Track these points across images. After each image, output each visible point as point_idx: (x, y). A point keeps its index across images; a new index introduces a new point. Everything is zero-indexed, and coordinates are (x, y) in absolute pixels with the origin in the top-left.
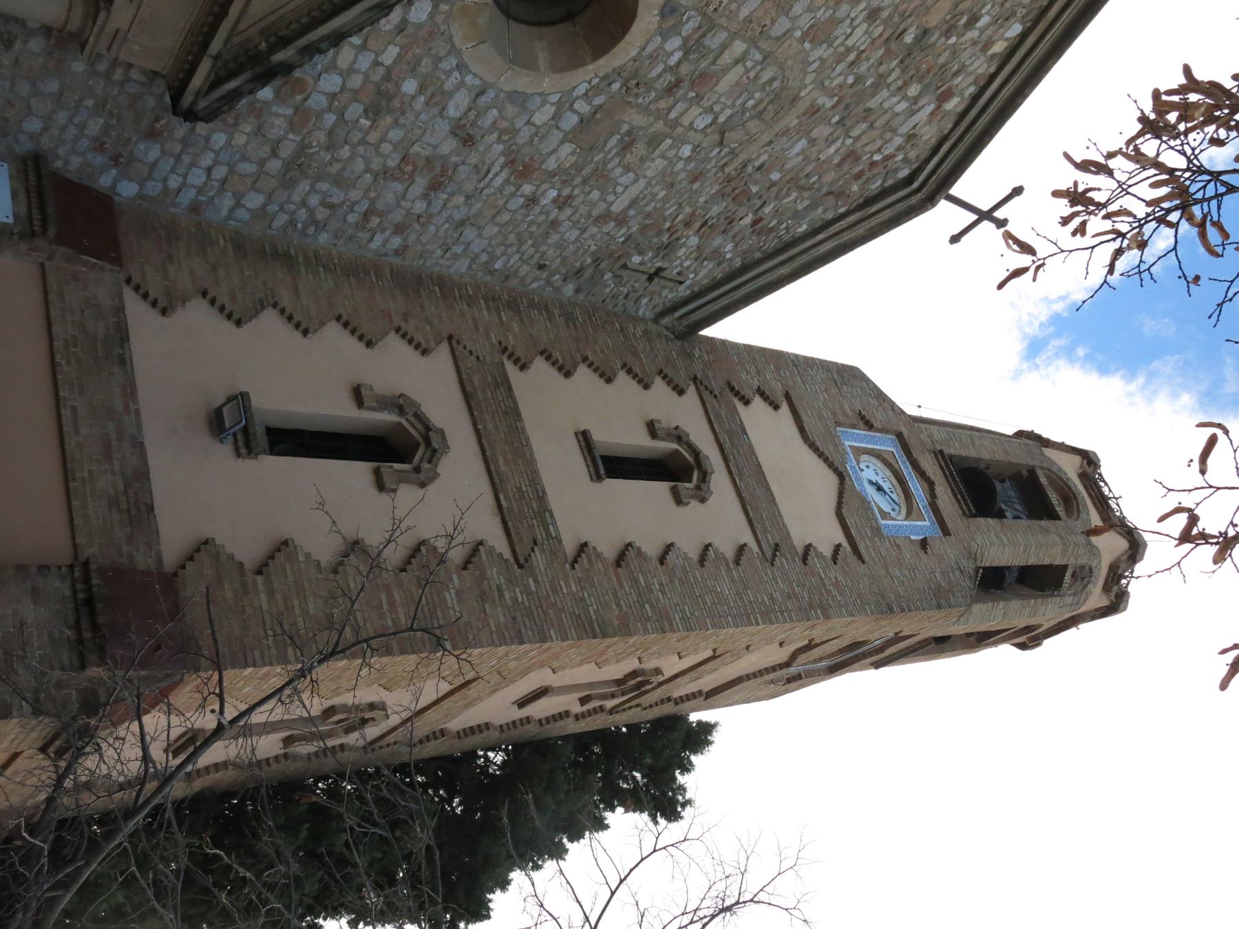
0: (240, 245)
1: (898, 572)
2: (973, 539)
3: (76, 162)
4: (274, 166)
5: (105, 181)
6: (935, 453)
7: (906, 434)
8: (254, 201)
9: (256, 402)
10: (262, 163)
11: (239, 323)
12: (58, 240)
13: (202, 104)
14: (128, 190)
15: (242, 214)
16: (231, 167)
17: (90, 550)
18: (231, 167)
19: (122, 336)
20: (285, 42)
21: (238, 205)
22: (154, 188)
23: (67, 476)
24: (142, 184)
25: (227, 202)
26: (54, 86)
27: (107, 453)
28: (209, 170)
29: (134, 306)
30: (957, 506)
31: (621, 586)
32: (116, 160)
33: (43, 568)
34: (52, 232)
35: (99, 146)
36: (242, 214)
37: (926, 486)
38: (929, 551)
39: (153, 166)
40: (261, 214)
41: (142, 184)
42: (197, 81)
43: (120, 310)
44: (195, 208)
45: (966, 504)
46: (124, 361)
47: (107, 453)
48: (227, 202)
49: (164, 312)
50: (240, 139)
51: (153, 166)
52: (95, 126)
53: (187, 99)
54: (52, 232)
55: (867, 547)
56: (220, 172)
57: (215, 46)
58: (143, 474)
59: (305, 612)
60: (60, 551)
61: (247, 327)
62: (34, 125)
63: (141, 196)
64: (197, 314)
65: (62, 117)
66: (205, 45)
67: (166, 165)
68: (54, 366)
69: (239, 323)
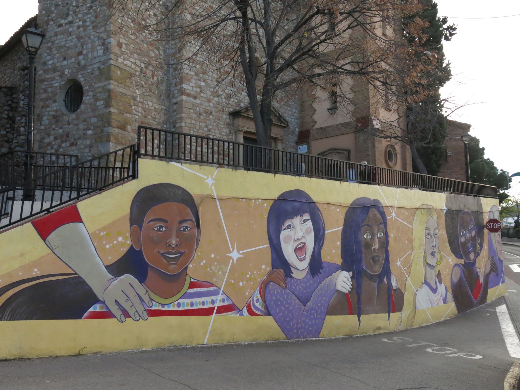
0: (302, 111)
3: (295, 138)
4: (289, 109)
5: (297, 133)
8: (294, 110)
9: (329, 107)
10: (289, 111)
11: (316, 110)
12: (308, 139)
13: (286, 123)
14: (297, 130)
15: (297, 112)
16: (291, 115)
17: (353, 131)
18: (291, 115)
19: (321, 128)
20: (276, 115)
21: (295, 112)
22: (296, 126)
23: (343, 134)
24: (296, 128)
25: (295, 114)
26: (287, 142)
27: (339, 129)
28: (292, 119)
29: (316, 126)
31: (357, 30)
32: (294, 132)
33: (355, 137)
34: (307, 140)
35: (293, 135)
36: (297, 112)
39: (293, 127)
40: (296, 109)
41: (296, 128)
42: (283, 125)
43: (317, 129)
44: (297, 119)
46: (325, 128)
47: (339, 129)
48: (295, 114)
49: (316, 122)
50: (287, 115)
51: (293, 127)
52: (290, 136)
53: (286, 126)
54: (307, 140)
56: (292, 117)
57: (279, 124)
58: (342, 124)
59: (362, 98)
60: (353, 134)
61: (316, 109)
62: (292, 144)
63: (298, 128)
64: (315, 117)
65: (290, 141)
66: (278, 125)
67: (293, 125)
68: (327, 137)
69: (316, 110)
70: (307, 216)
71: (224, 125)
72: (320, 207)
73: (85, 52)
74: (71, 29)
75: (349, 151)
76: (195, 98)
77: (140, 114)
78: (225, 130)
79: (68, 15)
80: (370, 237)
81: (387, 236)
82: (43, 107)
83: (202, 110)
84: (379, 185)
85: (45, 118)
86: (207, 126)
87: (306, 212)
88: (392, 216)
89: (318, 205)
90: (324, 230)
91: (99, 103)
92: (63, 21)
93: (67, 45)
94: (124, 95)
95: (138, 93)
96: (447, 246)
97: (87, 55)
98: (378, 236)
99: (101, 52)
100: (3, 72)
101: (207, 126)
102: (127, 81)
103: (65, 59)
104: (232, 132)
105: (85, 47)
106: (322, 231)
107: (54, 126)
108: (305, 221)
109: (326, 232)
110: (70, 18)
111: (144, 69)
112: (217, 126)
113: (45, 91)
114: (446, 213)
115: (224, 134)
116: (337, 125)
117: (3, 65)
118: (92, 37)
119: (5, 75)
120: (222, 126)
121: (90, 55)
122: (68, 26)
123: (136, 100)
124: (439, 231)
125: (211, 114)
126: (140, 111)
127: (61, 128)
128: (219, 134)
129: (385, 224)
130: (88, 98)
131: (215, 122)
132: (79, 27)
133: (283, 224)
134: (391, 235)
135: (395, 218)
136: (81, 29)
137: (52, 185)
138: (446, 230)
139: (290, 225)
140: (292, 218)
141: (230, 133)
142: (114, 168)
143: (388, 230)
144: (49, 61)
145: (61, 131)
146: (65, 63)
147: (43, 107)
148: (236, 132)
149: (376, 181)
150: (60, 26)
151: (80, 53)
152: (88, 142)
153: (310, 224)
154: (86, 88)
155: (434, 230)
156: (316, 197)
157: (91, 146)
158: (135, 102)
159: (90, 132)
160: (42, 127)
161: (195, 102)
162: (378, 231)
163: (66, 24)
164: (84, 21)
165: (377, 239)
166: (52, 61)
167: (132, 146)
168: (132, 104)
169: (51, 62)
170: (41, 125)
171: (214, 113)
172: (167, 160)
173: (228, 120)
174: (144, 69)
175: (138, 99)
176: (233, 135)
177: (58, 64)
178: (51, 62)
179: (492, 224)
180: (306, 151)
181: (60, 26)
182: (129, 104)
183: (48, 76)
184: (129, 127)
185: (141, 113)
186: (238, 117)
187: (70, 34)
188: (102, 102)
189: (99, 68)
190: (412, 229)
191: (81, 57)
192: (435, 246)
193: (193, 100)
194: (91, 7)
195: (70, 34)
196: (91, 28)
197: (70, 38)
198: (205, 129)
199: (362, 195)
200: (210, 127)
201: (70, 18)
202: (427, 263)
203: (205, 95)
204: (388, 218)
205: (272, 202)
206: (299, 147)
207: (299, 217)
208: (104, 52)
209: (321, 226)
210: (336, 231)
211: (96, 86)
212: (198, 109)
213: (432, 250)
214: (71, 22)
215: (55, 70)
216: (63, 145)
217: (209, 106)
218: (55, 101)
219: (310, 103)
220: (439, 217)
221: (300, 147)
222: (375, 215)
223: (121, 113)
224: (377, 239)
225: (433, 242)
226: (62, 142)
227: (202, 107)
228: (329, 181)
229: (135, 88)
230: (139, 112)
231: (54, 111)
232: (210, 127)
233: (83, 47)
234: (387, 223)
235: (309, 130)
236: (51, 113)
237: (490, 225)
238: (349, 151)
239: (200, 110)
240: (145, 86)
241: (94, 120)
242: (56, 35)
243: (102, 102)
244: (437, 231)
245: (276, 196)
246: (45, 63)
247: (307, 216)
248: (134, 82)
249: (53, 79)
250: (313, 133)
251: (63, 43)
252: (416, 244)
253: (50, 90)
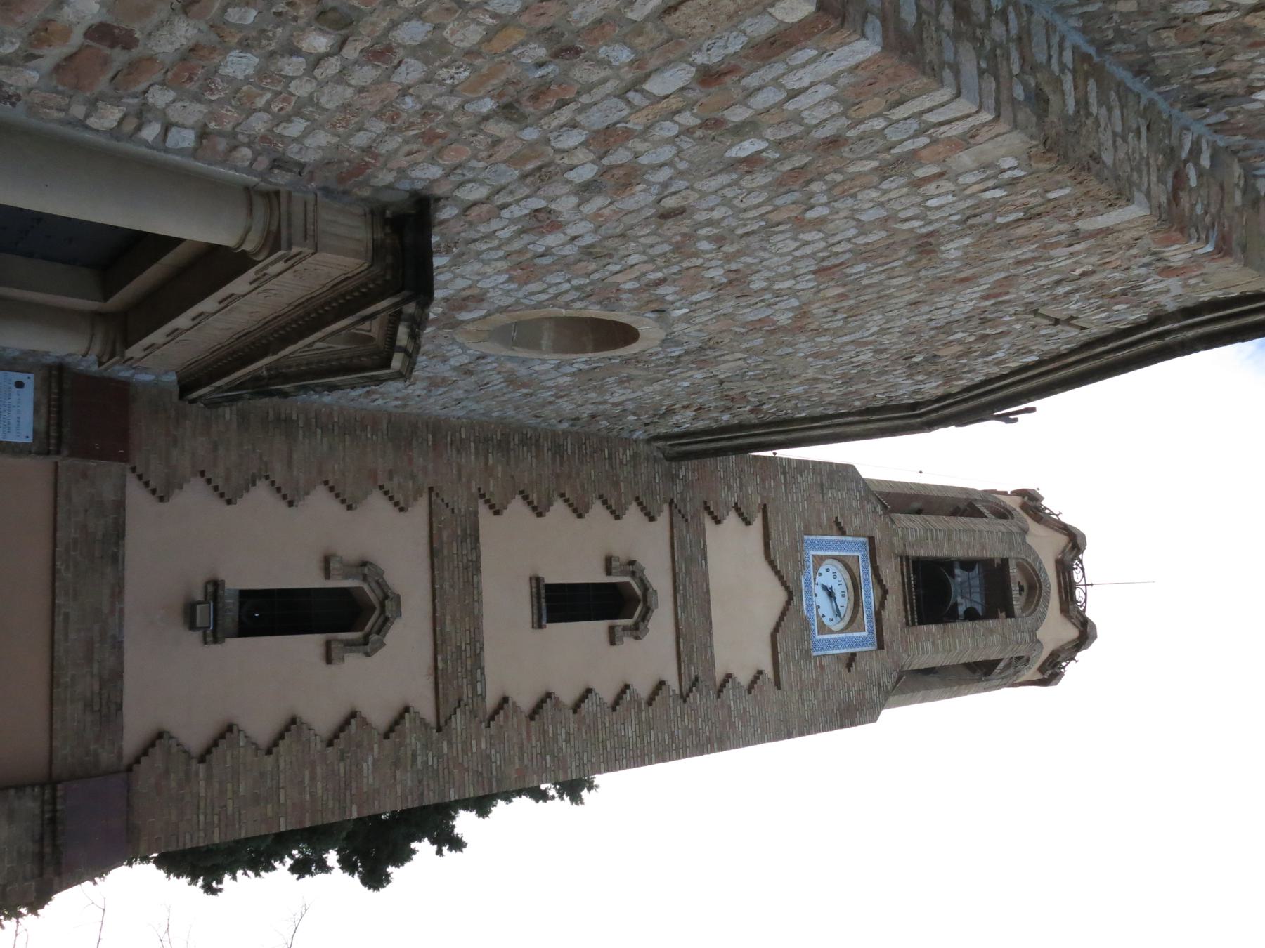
1: (811, 694)
2: (906, 650)
6: (901, 558)
7: (877, 541)
19: (118, 533)
23: (53, 682)
29: (136, 495)
30: (903, 614)
34: (65, 452)
37: (880, 592)
38: (853, 669)
43: (120, 506)
45: (912, 614)
46: (116, 560)
55: (789, 672)
58: (118, 674)
59: (235, 792)
64: (193, 496)
68: (54, 572)
71: (367, 150)
76: (709, 77)
78: (322, 139)
83: (582, 72)
104: (281, 179)
112: (388, 112)
115: (296, 128)
116: (118, 646)
120: (361, 139)
125: (509, 111)
128: (311, 100)
131: (427, 112)
141: (279, 163)
148: (272, 197)
161: (684, 58)
171: (499, 128)
172: (1079, 541)
173: (386, 178)
176: (250, 170)
186: (377, 250)
193: (711, 57)
198: (413, 33)
200: (412, 71)
206: (29, 380)
212: (623, 55)
217: (574, 125)
219: (279, 475)
221: (28, 394)
227: (610, 86)
235: (124, 458)
239: (605, 63)
250: (105, 474)
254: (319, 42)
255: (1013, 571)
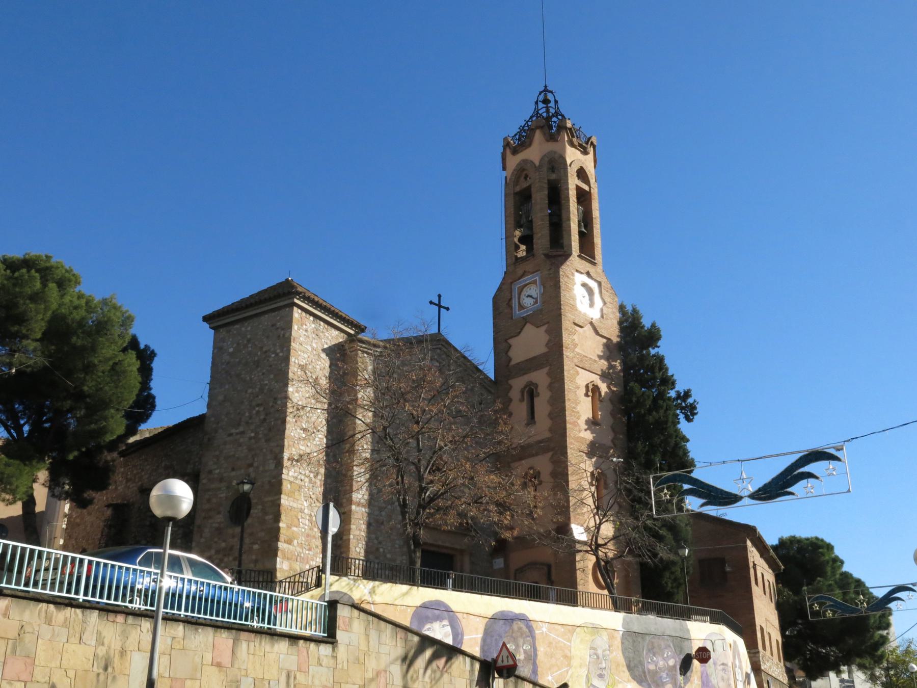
70: (446, 622)
72: (460, 616)
73: (255, 464)
74: (241, 440)
75: (549, 567)
77: (306, 527)
79: (239, 425)
80: (514, 648)
81: (535, 649)
82: (205, 518)
84: (583, 607)
85: (207, 530)
86: (377, 538)
87: (446, 619)
88: (541, 631)
89: (457, 614)
90: (463, 635)
91: (267, 518)
92: (233, 431)
93: (237, 456)
94: (292, 508)
95: (306, 505)
96: (624, 672)
97: (258, 467)
98: (524, 648)
99: (272, 466)
100: (139, 467)
101: (377, 538)
102: (296, 493)
103: (233, 469)
105: (256, 459)
106: (460, 636)
107: (216, 540)
108: (444, 626)
109: (465, 637)
110: (241, 429)
111: (313, 479)
113: (209, 500)
114: (623, 635)
117: (141, 458)
118: (264, 450)
119: (143, 470)
121: (261, 468)
122: (239, 436)
123: (304, 513)
124: (611, 653)
126: (307, 524)
127: (224, 541)
129: (533, 637)
130: (256, 511)
132: (250, 438)
133: (424, 627)
134: (541, 649)
135: (546, 634)
136: (253, 441)
137: (297, 583)
138: (623, 653)
139: (430, 628)
140: (432, 623)
142: (381, 569)
143: (537, 644)
144: (215, 469)
145: (223, 545)
146: (233, 474)
147: (205, 518)
149: (577, 603)
150: (231, 435)
151: (250, 465)
152: (254, 557)
153: (448, 629)
154: (254, 501)
155: (604, 651)
156: (454, 608)
157: (256, 561)
158: (302, 514)
159: (256, 547)
160: (203, 540)
162: (524, 644)
163: (237, 434)
164: (257, 433)
165: (522, 650)
166: (218, 470)
167: (318, 567)
168: (300, 517)
169: (217, 471)
170: (201, 537)
174: (313, 479)
175: (306, 511)
177: (225, 475)
178: (217, 471)
179: (701, 653)
180: (502, 566)
181: (231, 435)
182: (297, 517)
183: (213, 486)
184: (295, 542)
185: (308, 526)
187: (240, 445)
188: (271, 517)
189: (270, 482)
190: (571, 646)
191: (251, 470)
192: (605, 668)
194: (265, 420)
195: (240, 445)
196: (263, 440)
197: (240, 449)
199: (505, 609)
200: (381, 539)
201: (241, 429)
202: (591, 684)
203: (376, 504)
204: (537, 632)
205: (415, 609)
207: (438, 622)
208: (276, 467)
209: (460, 631)
210: (475, 638)
211: (266, 499)
213: (599, 672)
214: (243, 433)
215: (221, 480)
216: (226, 559)
218: (219, 513)
220: (611, 637)
222: (520, 628)
223: (289, 527)
224: (522, 650)
225: (601, 663)
226: (225, 555)
228: (469, 594)
229: (303, 500)
230: (306, 525)
231: (218, 523)
232: (381, 539)
233: (254, 459)
234: (535, 637)
236: (214, 525)
237: (699, 655)
238: (549, 567)
240: (313, 496)
241: (261, 534)
242: (225, 443)
243: (271, 517)
244: (607, 652)
245: (419, 603)
246: (210, 472)
247: (446, 622)
248: (302, 494)
249: (219, 489)
251: (232, 453)
252: (575, 662)
253: (214, 500)
254: (381, 550)
255: (518, 189)
